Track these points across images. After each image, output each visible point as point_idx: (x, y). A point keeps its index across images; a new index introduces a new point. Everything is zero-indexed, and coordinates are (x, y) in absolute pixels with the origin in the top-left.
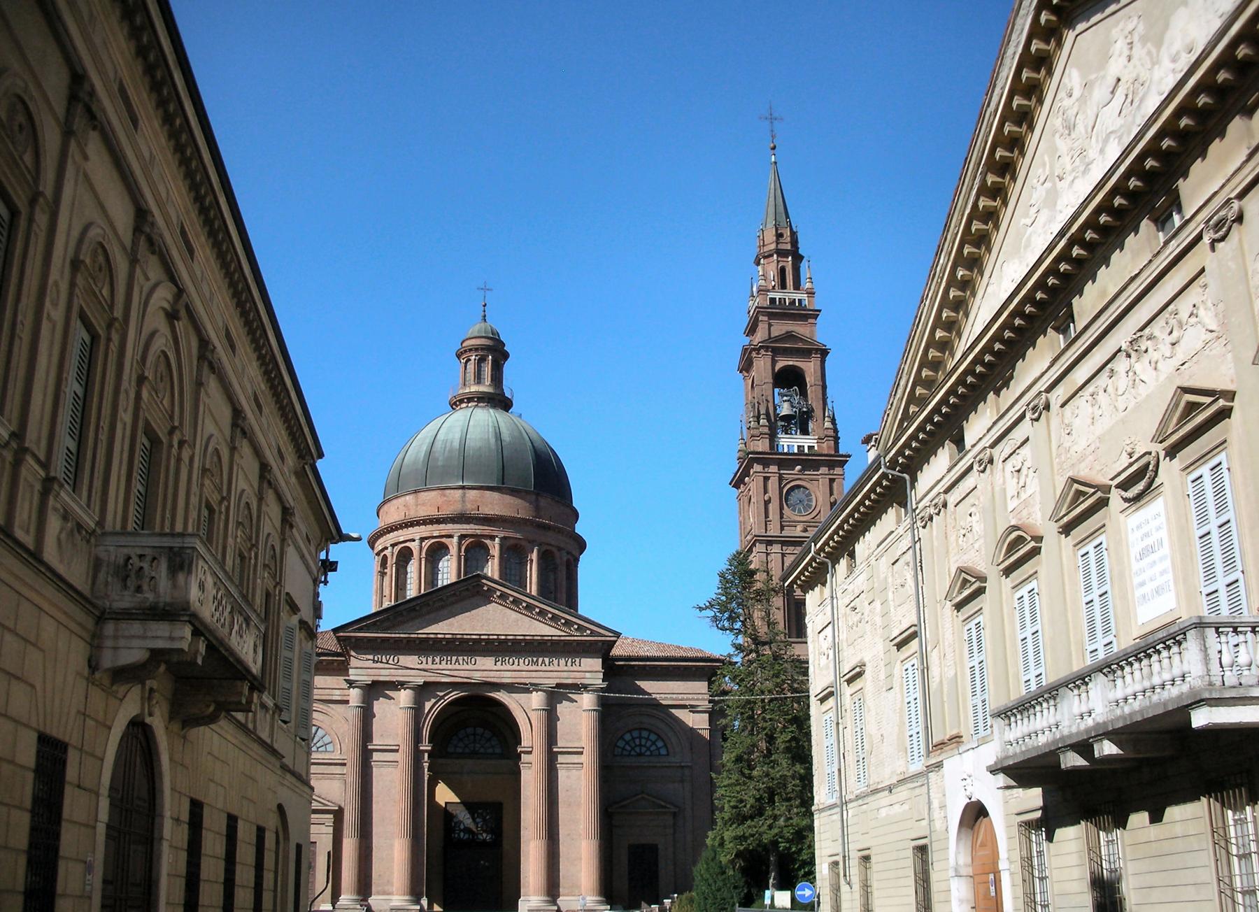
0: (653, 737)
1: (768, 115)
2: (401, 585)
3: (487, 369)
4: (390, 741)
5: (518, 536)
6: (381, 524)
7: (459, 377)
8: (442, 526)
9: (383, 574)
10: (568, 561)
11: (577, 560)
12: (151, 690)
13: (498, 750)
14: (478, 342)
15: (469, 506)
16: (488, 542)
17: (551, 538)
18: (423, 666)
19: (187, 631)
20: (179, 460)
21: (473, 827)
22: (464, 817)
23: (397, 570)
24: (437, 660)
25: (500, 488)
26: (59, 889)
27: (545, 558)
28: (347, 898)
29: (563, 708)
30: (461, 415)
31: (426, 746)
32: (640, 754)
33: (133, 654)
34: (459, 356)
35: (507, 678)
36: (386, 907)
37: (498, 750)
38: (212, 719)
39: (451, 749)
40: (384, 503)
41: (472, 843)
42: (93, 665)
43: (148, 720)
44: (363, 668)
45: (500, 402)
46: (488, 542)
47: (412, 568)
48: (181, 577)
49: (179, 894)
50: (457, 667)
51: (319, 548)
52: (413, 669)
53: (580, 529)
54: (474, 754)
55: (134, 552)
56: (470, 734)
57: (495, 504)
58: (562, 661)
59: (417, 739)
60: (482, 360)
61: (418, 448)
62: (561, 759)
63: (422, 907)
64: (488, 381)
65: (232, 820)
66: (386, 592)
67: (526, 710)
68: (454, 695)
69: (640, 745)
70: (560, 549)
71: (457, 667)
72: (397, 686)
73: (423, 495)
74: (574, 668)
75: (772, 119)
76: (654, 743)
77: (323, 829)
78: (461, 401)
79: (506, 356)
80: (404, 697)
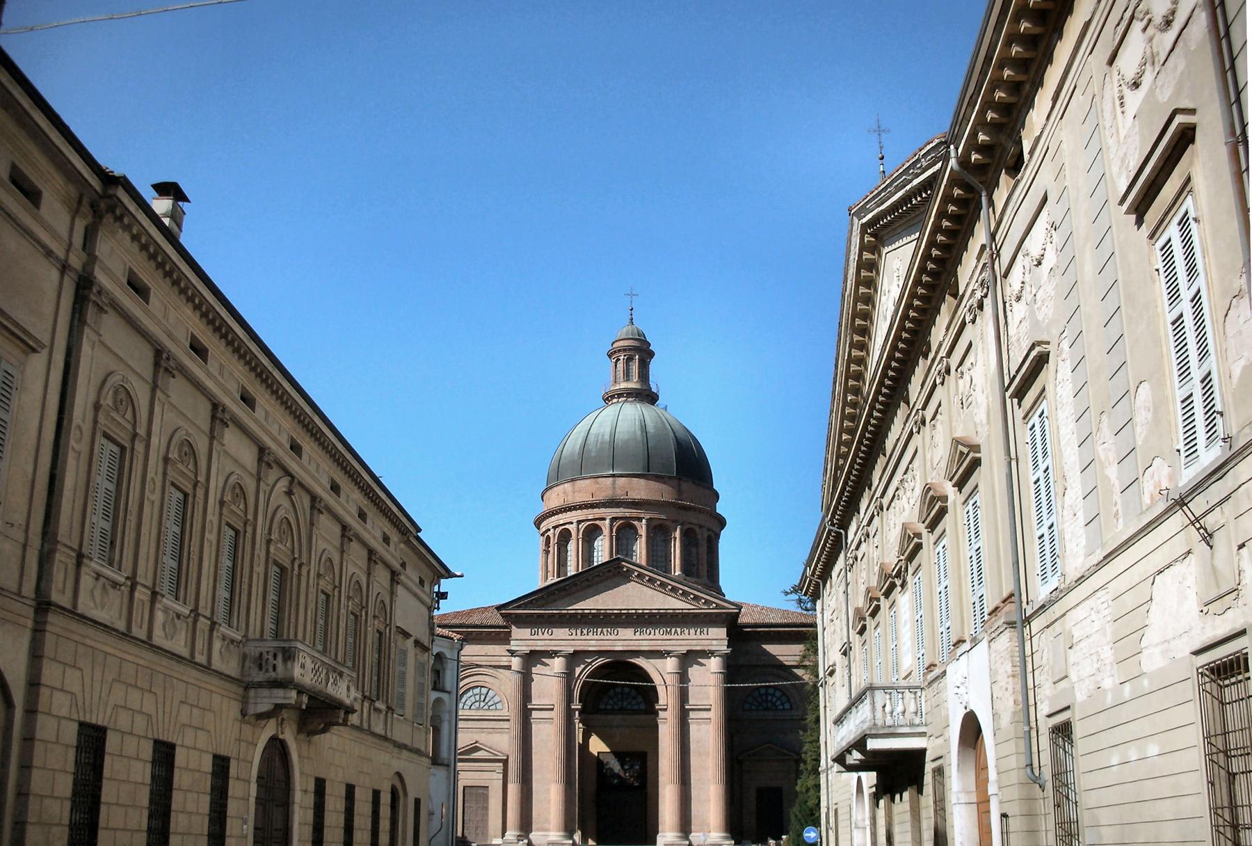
0: (784, 698)
1: (875, 127)
2: (562, 563)
3: (635, 367)
4: (546, 702)
5: (663, 517)
6: (543, 508)
7: (606, 375)
8: (596, 510)
9: (547, 552)
10: (709, 537)
11: (718, 536)
12: (283, 720)
13: (643, 707)
14: (626, 343)
15: (619, 492)
16: (635, 523)
17: (692, 518)
18: (573, 637)
19: (294, 694)
20: (299, 575)
21: (622, 774)
22: (615, 766)
23: (559, 549)
24: (585, 631)
25: (647, 474)
26: (228, 833)
27: (688, 537)
28: (511, 834)
29: (694, 671)
30: (612, 410)
31: (577, 705)
32: (767, 709)
33: (264, 707)
34: (610, 356)
35: (645, 646)
36: (544, 841)
37: (643, 707)
38: (324, 731)
39: (602, 707)
40: (547, 490)
41: (623, 785)
42: (244, 713)
43: (281, 737)
44: (523, 639)
45: (647, 396)
46: (635, 523)
47: (571, 547)
48: (289, 663)
49: (308, 831)
50: (602, 637)
51: (433, 583)
52: (564, 639)
53: (721, 508)
54: (622, 711)
55: (264, 650)
56: (615, 695)
57: (641, 489)
58: (692, 631)
59: (569, 699)
60: (629, 360)
61: (574, 443)
62: (692, 715)
63: (574, 842)
64: (635, 377)
65: (350, 790)
66: (550, 568)
67: (662, 672)
68: (601, 661)
69: (767, 701)
70: (701, 527)
71: (602, 637)
72: (552, 654)
73: (580, 483)
74: (703, 637)
75: (879, 131)
76: (779, 699)
77: (495, 775)
78: (613, 397)
79: (652, 354)
80: (558, 664)
